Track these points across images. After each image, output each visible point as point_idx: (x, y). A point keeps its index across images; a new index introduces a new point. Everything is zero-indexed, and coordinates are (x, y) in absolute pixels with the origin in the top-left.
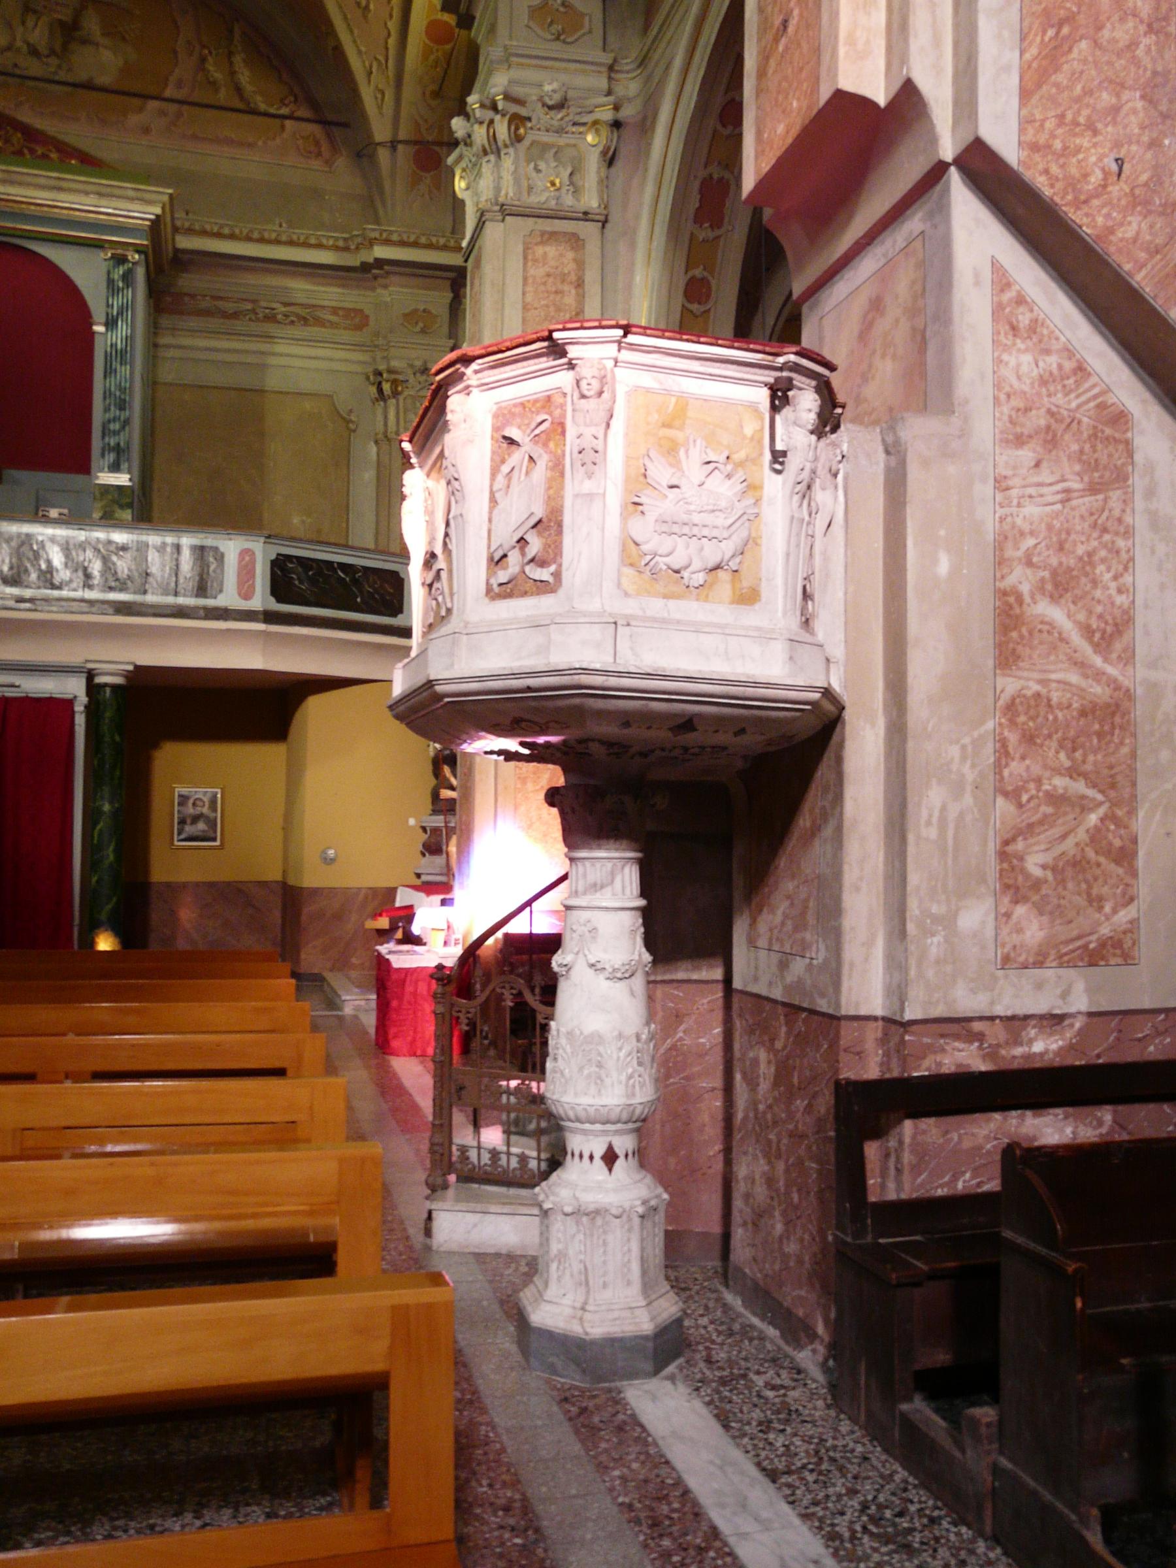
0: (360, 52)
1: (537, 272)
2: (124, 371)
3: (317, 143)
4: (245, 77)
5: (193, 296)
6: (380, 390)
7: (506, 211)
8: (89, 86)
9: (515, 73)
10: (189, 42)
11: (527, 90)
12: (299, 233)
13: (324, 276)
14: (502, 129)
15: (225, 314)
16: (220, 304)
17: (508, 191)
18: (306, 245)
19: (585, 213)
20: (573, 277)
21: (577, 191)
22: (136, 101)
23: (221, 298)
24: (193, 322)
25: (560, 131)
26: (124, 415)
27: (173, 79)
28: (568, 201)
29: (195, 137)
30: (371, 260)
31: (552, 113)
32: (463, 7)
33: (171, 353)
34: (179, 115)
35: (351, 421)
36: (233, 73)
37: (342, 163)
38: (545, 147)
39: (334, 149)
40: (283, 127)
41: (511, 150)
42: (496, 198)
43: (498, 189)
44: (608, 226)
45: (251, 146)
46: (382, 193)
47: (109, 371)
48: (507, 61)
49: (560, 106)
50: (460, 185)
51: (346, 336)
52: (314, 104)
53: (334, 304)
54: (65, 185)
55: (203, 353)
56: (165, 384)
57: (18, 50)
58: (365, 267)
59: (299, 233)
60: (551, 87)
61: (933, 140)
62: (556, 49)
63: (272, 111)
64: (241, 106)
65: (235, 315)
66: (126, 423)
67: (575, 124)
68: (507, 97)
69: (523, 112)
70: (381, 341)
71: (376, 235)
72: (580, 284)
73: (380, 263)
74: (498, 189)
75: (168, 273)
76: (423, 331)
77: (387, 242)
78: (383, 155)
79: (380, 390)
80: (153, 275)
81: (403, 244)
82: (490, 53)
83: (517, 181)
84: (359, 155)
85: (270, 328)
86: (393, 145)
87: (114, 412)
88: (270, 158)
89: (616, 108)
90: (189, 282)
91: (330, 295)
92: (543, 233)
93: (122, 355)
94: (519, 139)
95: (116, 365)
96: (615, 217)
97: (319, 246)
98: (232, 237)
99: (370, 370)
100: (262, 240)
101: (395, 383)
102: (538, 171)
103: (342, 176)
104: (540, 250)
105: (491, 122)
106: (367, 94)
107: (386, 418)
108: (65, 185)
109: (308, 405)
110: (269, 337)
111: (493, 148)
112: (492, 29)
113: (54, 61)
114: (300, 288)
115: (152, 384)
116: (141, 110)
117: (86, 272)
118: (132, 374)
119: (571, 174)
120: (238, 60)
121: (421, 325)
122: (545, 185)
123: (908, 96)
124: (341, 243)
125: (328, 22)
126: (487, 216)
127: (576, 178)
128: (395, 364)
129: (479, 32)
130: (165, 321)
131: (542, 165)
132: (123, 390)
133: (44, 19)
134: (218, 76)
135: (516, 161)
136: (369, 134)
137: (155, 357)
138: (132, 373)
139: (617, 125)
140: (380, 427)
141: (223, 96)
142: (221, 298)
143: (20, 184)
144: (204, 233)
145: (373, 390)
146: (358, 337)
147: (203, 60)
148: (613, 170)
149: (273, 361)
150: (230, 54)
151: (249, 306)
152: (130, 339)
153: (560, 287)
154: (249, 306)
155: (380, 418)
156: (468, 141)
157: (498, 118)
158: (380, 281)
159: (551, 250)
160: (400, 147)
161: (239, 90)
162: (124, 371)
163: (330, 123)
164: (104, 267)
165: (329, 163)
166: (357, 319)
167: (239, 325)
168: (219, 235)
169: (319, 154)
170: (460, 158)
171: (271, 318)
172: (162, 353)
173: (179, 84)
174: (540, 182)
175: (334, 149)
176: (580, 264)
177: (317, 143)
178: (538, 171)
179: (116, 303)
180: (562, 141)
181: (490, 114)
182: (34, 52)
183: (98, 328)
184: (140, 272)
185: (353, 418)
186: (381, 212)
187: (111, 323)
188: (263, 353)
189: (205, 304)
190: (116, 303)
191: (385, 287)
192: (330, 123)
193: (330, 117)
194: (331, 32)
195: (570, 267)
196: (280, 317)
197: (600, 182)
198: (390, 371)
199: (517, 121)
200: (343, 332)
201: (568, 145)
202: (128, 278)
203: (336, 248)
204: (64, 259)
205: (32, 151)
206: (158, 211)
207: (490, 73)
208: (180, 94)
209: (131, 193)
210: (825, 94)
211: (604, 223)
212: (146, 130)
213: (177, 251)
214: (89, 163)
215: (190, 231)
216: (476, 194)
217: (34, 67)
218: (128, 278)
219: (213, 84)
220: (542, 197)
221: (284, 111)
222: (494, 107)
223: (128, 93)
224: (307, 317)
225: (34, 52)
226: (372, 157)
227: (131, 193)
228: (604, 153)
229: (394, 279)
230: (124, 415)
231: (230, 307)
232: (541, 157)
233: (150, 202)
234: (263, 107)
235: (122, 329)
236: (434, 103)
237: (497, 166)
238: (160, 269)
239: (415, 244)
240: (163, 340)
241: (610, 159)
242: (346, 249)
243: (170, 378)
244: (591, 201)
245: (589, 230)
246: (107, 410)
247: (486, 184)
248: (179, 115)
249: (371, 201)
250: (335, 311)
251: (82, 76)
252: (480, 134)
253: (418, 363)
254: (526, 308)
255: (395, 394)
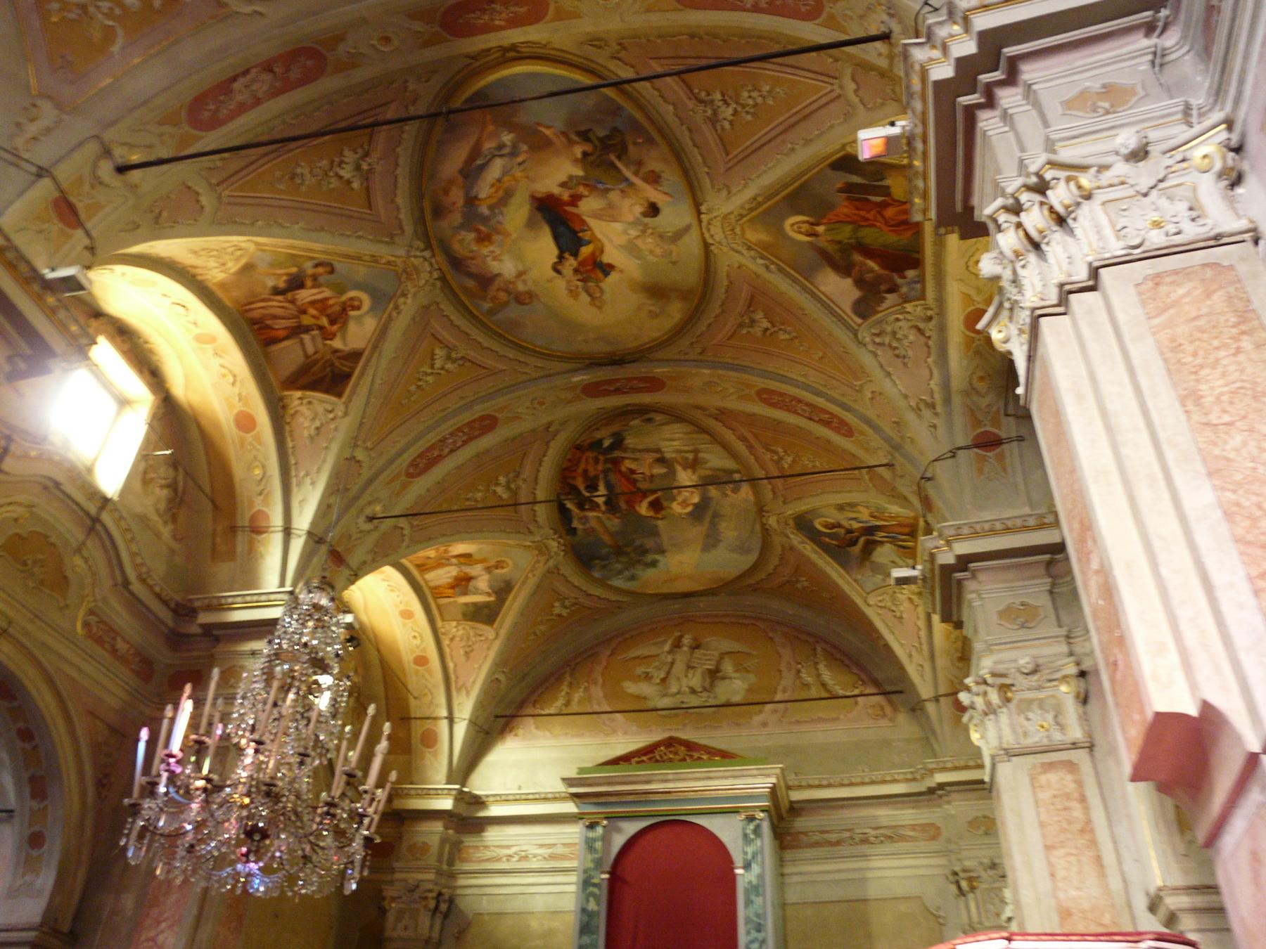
0: (902, 645)
1: (1045, 795)
2: (758, 901)
3: (882, 708)
4: (827, 676)
5: (805, 833)
6: (959, 888)
7: (1010, 754)
8: (728, 705)
9: (996, 657)
10: (789, 663)
11: (1006, 666)
12: (877, 775)
13: (903, 802)
14: (994, 697)
15: (830, 843)
16: (825, 836)
17: (1009, 739)
18: (884, 782)
19: (1074, 744)
20: (1076, 795)
21: (1062, 727)
22: (757, 708)
23: (827, 832)
24: (808, 853)
25: (1039, 688)
26: (761, 936)
27: (780, 688)
28: (1057, 737)
29: (798, 722)
30: (934, 785)
31: (1029, 677)
32: (955, 618)
33: (796, 879)
34: (786, 709)
35: (939, 917)
36: (819, 675)
37: (902, 718)
38: (1031, 701)
39: (895, 710)
40: (856, 703)
41: (1004, 710)
42: (1001, 743)
43: (1000, 738)
44: (1095, 749)
45: (836, 719)
46: (934, 732)
47: (748, 902)
48: (989, 649)
49: (1034, 672)
50: (975, 736)
51: (925, 846)
52: (876, 683)
53: (912, 822)
54: (712, 775)
55: (817, 874)
56: (793, 904)
57: (684, 693)
58: (931, 791)
59: (877, 775)
60: (1024, 661)
61: (1238, 739)
62: (1023, 634)
63: (848, 694)
64: (825, 695)
65: (838, 843)
66: (763, 942)
67: (1050, 681)
68: (994, 675)
69: (1007, 681)
70: (954, 847)
71: (934, 766)
72: (1083, 799)
73: (941, 786)
74: (1000, 738)
75: (785, 821)
76: (986, 834)
77: (944, 769)
78: (931, 707)
79: (959, 888)
80: (775, 821)
81: (957, 768)
82: (978, 646)
83: (1014, 731)
84: (913, 710)
85: (865, 849)
86: (936, 699)
87: (754, 934)
88: (855, 723)
89: (1078, 664)
90: (801, 823)
91: (907, 816)
92: (1043, 764)
93: (755, 889)
94: (1009, 700)
95: (753, 897)
96: (1099, 739)
97: (894, 781)
98: (829, 786)
99: (948, 872)
100: (851, 785)
101: (970, 880)
102: (1028, 719)
103: (904, 726)
104: (1043, 779)
105: (985, 693)
106: (911, 669)
107: (969, 911)
108: (712, 775)
109: (903, 907)
110: (865, 856)
111: (990, 710)
112: (976, 631)
113: (705, 694)
114: (884, 814)
115: (782, 906)
116: (761, 712)
117: (727, 831)
118: (765, 903)
119: (1056, 717)
120: (822, 667)
121: (983, 828)
122: (1037, 728)
123: (1206, 707)
124: (909, 776)
125: (877, 631)
126: (997, 759)
127: (1060, 719)
128: (968, 864)
129: (968, 631)
130: (788, 855)
131: (1031, 715)
132: (758, 915)
133: (699, 671)
134: (809, 679)
135: (1010, 718)
136: (918, 695)
137: (783, 883)
138: (765, 902)
139: (1082, 674)
140: (965, 920)
141: (814, 692)
142: (827, 832)
143: (684, 780)
144: (810, 787)
145: (953, 888)
146: (934, 846)
147: (799, 671)
148: (1089, 706)
149: (870, 874)
150: (816, 664)
151: (847, 834)
152: (761, 877)
153: (1067, 804)
154: (847, 834)
155: (964, 911)
156: (972, 707)
157: (989, 689)
158: (945, 798)
159: (1053, 777)
160: (942, 699)
161: (824, 685)
162: (758, 901)
163: (889, 693)
164: (740, 825)
165: (892, 720)
166: (931, 832)
167: (842, 850)
168: (820, 786)
169: (884, 716)
170: (971, 718)
171: (865, 841)
172: (787, 880)
173: (785, 690)
174: (1031, 727)
175: (895, 710)
176: (1079, 783)
177: (882, 708)
178: (1028, 719)
179: (750, 850)
180: (1041, 695)
181: (984, 687)
182: (693, 691)
183: (739, 871)
184: (766, 827)
185: (942, 914)
186: (936, 746)
187: (747, 866)
188: (862, 869)
189: (817, 837)
190: (750, 850)
191: (949, 803)
192: (889, 693)
193: (889, 688)
194: (880, 637)
195: (1072, 787)
196: (872, 839)
197: (1080, 718)
198: (965, 871)
199: (1004, 688)
200: (923, 843)
201: (1048, 697)
202: (757, 831)
203: (907, 780)
204: (712, 824)
205: (691, 756)
206: (774, 780)
207: (979, 659)
208: (786, 696)
209: (755, 772)
210: (1149, 716)
211: (1091, 748)
212: (765, 724)
213: (791, 802)
214: (726, 756)
215: (800, 787)
216: (987, 743)
217: (694, 701)
218: (757, 831)
219: (807, 686)
220: (1036, 738)
221: (856, 692)
222: (985, 682)
223: (753, 703)
224: (893, 836)
225: (693, 691)
226: (922, 709)
227: (755, 772)
228: (1077, 697)
229: (954, 796)
230: (761, 936)
231: (833, 837)
232: (1029, 709)
233: (768, 776)
234: (841, 692)
235: (756, 869)
236: (960, 665)
237: (997, 722)
238: (781, 818)
239: (966, 767)
240: (787, 870)
241: (1084, 700)
242: (914, 780)
243: (794, 900)
244: (1076, 733)
245: (1080, 756)
246: (748, 933)
247: (992, 734)
248: (786, 709)
249: (928, 741)
250: (913, 827)
251: (722, 699)
252: (979, 702)
253: (986, 861)
254: (1042, 825)
255: (973, 889)
